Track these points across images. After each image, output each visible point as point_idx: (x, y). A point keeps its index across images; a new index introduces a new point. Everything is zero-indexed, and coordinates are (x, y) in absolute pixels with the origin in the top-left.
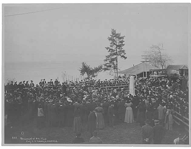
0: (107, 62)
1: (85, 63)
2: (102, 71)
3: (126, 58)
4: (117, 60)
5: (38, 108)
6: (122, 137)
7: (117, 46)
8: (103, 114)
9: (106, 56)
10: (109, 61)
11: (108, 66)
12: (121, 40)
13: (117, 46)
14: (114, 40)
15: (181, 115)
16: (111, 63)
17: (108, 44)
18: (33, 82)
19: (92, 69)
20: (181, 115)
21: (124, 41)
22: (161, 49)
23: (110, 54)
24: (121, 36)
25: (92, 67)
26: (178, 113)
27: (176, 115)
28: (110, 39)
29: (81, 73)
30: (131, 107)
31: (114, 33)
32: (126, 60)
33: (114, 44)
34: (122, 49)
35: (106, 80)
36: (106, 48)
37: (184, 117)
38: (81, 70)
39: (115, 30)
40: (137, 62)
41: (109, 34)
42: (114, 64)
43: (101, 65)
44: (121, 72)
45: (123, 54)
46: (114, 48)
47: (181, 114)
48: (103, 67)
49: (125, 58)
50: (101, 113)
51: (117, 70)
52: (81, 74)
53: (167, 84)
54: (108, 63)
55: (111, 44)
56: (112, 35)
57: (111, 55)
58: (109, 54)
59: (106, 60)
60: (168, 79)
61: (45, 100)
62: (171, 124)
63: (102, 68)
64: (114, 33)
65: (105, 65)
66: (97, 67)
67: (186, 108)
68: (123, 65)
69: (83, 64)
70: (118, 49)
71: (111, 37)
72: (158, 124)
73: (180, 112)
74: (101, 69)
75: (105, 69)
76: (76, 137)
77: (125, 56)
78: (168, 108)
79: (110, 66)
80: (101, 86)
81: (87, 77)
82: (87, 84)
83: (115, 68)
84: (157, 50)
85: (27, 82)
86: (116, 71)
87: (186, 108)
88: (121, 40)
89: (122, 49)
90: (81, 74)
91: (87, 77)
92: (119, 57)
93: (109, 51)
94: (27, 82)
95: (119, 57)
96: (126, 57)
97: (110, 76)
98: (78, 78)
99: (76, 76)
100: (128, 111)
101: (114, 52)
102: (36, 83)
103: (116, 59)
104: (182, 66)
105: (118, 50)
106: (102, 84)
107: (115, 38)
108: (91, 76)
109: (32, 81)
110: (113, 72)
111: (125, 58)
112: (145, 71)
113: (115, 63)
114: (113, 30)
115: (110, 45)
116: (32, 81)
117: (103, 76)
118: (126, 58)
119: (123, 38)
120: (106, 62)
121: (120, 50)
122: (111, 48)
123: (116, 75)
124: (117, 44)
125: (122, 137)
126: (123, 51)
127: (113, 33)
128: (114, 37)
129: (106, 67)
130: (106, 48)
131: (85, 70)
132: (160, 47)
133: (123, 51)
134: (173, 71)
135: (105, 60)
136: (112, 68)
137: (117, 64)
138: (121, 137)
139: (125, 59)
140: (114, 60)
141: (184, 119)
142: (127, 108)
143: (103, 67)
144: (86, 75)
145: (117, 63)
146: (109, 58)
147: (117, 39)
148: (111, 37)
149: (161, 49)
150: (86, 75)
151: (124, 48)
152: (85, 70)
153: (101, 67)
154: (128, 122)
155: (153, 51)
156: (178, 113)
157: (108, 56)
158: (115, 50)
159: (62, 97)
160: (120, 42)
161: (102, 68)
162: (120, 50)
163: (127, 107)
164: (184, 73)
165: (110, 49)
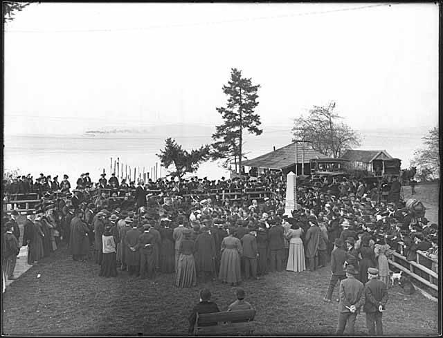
0: (218, 140)
1: (172, 140)
2: (208, 159)
3: (261, 131)
4: (241, 135)
5: (103, 236)
6: (287, 303)
7: (242, 106)
8: (239, 253)
9: (218, 128)
10: (225, 138)
11: (220, 149)
12: (251, 94)
13: (242, 106)
14: (235, 94)
15: (404, 258)
16: (227, 142)
17: (224, 100)
18: (68, 180)
19: (187, 153)
20: (404, 258)
21: (257, 97)
22: (333, 116)
23: (226, 122)
24: (253, 85)
25: (188, 148)
26: (397, 254)
27: (393, 257)
28: (227, 91)
29: (162, 162)
30: (300, 239)
31: (236, 75)
32: (259, 136)
33: (237, 101)
34: (252, 114)
35: (223, 178)
36: (217, 109)
37: (413, 262)
38: (162, 154)
39: (238, 70)
40: (284, 139)
41: (226, 79)
42: (234, 145)
43: (207, 146)
44: (248, 163)
45: (254, 123)
46: (235, 110)
47: (406, 256)
48: (212, 150)
49: (259, 132)
50: (234, 251)
51: (240, 159)
52: (163, 163)
53: (358, 190)
54: (221, 143)
55: (230, 101)
56: (232, 82)
57: (228, 124)
58: (222, 122)
59: (217, 136)
60: (361, 181)
61: (110, 219)
62: (383, 277)
63: (208, 153)
64: (236, 75)
65: (215, 146)
66: (198, 150)
67: (416, 243)
68: (253, 147)
69: (169, 141)
70: (244, 112)
71: (229, 86)
72: (375, 278)
73: (402, 252)
74: (207, 155)
75: (216, 156)
76: (201, 300)
77: (259, 128)
78: (378, 243)
79: (226, 149)
80: (234, 195)
81: (175, 170)
82: (184, 187)
83: (238, 152)
84: (324, 118)
85: (56, 178)
86: (238, 160)
87: (416, 243)
88: (251, 94)
89: (252, 114)
90: (163, 163)
91: (175, 170)
92: (245, 130)
93: (225, 115)
94: (56, 178)
95: (245, 130)
96: (260, 129)
97: (225, 170)
98: (148, 173)
99: (143, 165)
100: (296, 245)
101: (235, 119)
102: (35, 177)
103: (239, 134)
104: (378, 152)
105: (244, 115)
106: (214, 186)
107: (238, 88)
108: (184, 169)
109: (66, 177)
110: (232, 162)
111: (259, 132)
112: (300, 162)
113: (237, 142)
114: (235, 70)
115: (228, 103)
116: (66, 177)
117: (212, 171)
118: (261, 131)
119: (255, 88)
120: (216, 139)
121: (247, 115)
122: (229, 110)
123: (238, 169)
124: (244, 102)
125: (287, 303)
126: (256, 118)
127: (234, 77)
128: (237, 86)
129: (217, 151)
130: (217, 109)
131: (173, 154)
132: (333, 112)
133: (256, 118)
134: (358, 165)
135: (214, 135)
136: (231, 154)
137: (240, 145)
138: (282, 302)
139: (257, 134)
140: (235, 137)
141: (413, 266)
142: (293, 241)
143: (212, 150)
144: (173, 168)
145: (241, 142)
146: (225, 132)
147: (243, 91)
148: (229, 86)
149: (333, 116)
150: (173, 168)
151: (256, 111)
152: (172, 157)
153: (206, 150)
154: (296, 271)
155: (315, 120)
156: (397, 254)
157: (222, 126)
158: (238, 113)
159: (143, 214)
160: (250, 97)
161: (208, 153)
162: (247, 115)
163: (292, 237)
164: (382, 169)
165: (226, 112)
